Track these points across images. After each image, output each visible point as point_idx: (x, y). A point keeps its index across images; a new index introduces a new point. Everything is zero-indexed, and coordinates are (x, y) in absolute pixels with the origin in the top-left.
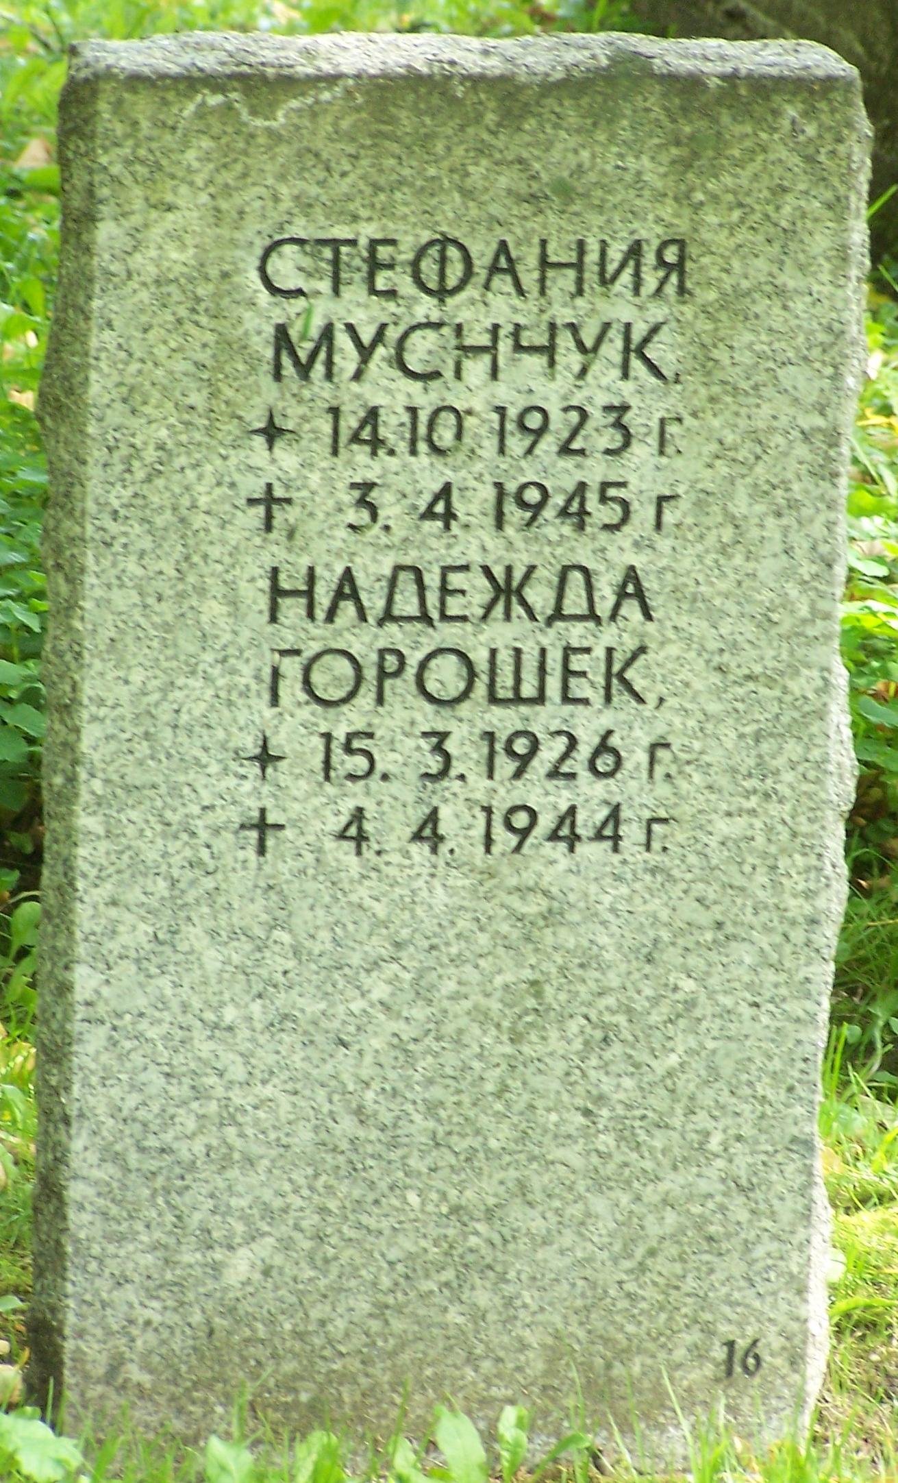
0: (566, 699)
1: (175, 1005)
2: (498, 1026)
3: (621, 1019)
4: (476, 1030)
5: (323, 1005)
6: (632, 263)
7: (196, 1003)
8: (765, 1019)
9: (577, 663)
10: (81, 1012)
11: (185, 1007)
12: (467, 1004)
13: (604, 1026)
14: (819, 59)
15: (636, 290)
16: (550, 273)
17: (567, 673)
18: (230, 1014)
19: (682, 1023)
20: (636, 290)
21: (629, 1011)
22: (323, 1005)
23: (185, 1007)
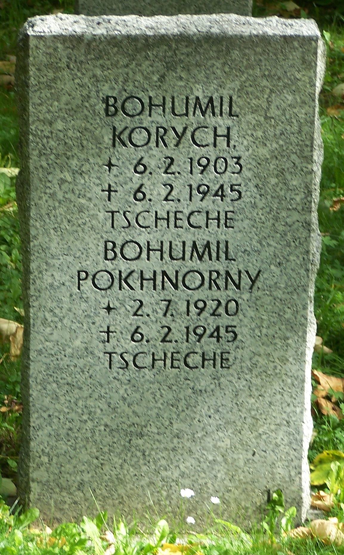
0: (176, 226)
1: (102, 5)
2: (175, 8)
3: (203, 6)
4: (170, 9)
5: (135, 4)
6: (207, 249)
7: (106, 4)
8: (236, 5)
9: (179, 215)
10: (81, 7)
11: (104, 5)
12: (168, 3)
13: (199, 7)
14: (307, 27)
15: (210, 259)
16: (160, 248)
17: (176, 219)
18: (114, 6)
19: (217, 7)
20: (210, 259)
21: (205, 4)
22: (135, 4)
23: (104, 5)
